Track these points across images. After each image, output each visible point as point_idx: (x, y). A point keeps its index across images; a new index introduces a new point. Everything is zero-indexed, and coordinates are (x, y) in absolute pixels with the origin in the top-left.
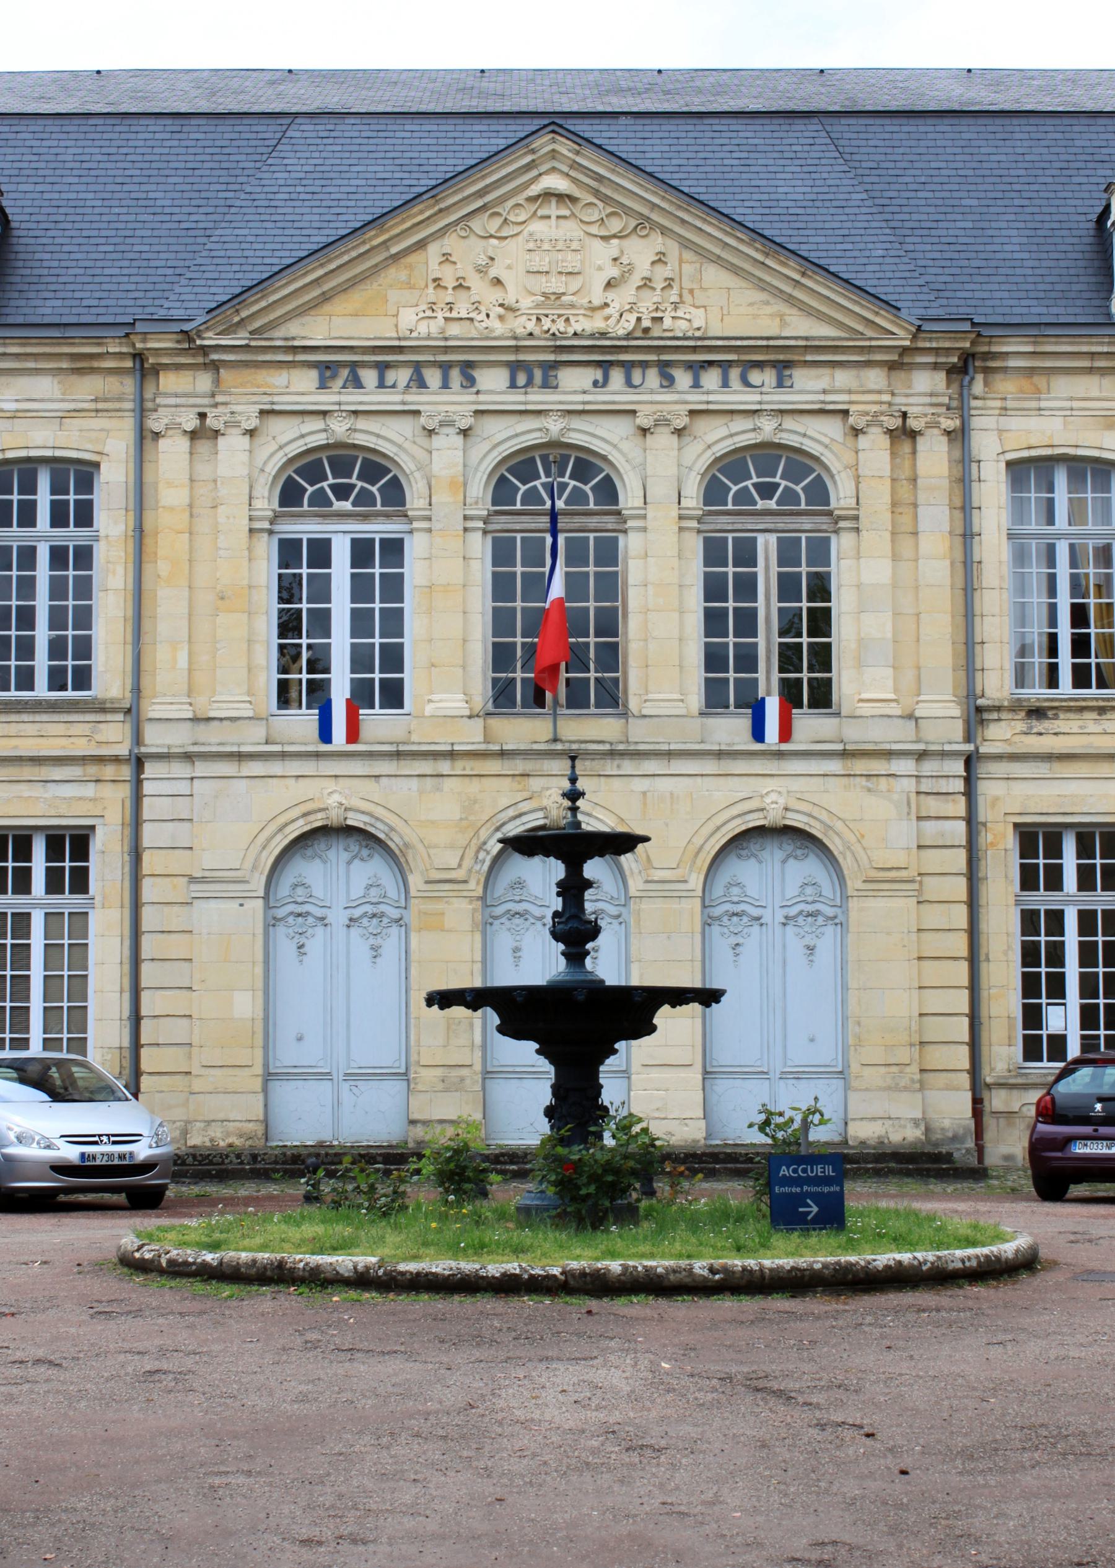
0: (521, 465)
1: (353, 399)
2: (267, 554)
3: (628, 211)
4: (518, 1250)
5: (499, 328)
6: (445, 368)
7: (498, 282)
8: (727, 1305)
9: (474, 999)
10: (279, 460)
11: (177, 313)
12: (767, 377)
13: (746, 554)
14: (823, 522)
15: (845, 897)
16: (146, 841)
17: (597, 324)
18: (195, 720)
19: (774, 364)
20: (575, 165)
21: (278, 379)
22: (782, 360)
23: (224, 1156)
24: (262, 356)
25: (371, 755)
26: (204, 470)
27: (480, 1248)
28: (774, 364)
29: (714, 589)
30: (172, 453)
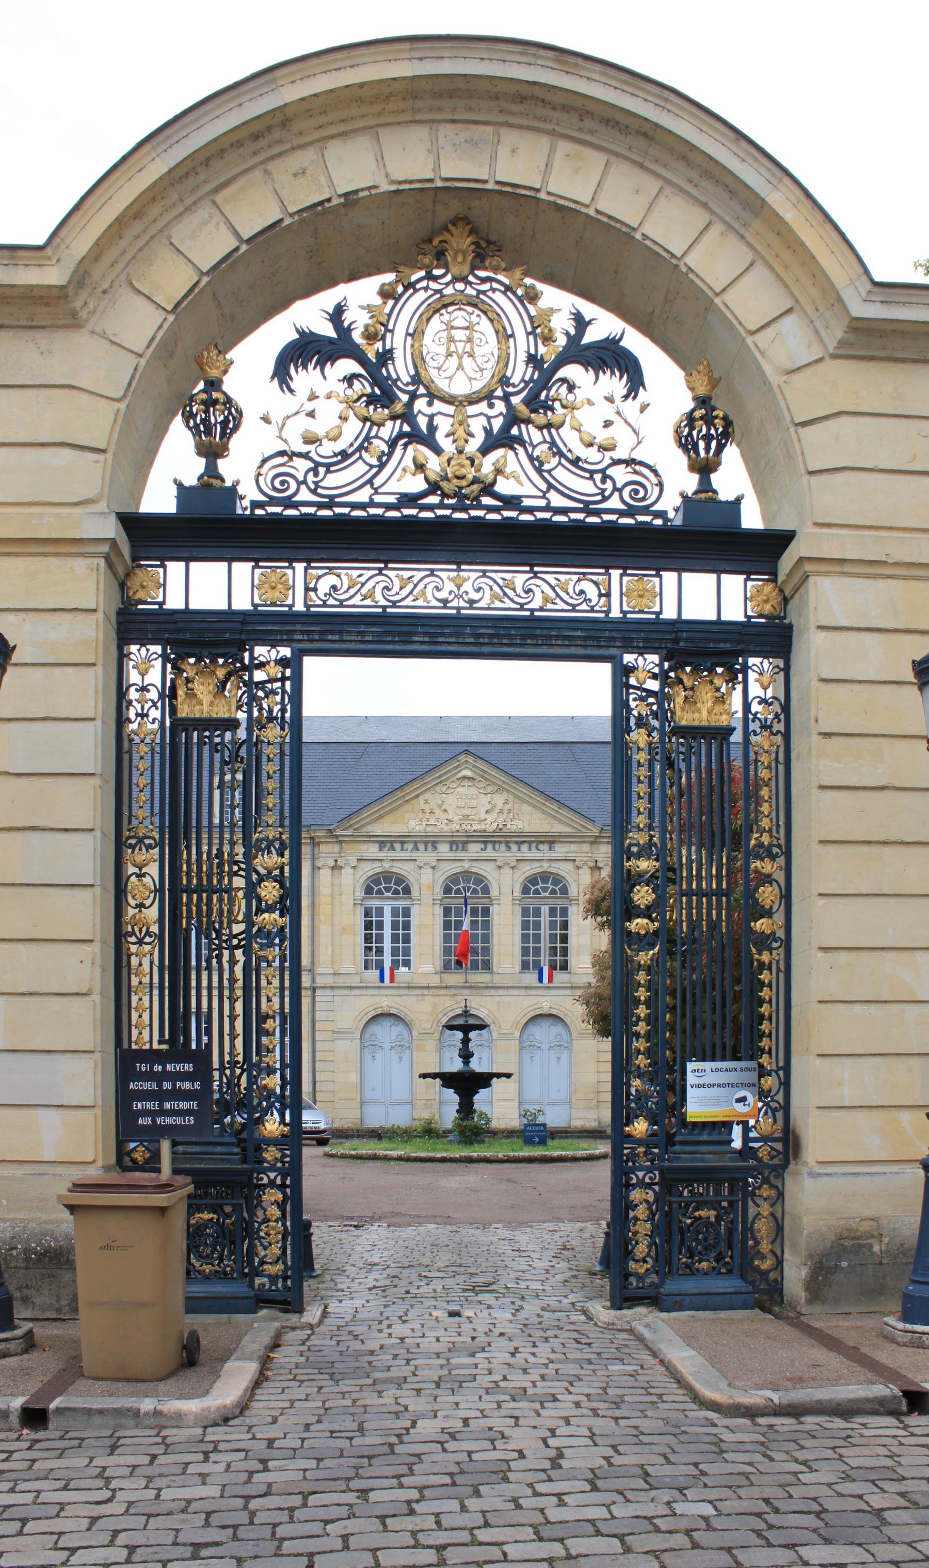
0: (454, 879)
1: (392, 855)
2: (360, 912)
3: (494, 784)
4: (446, 1151)
5: (446, 828)
6: (426, 843)
7: (445, 810)
8: (508, 1165)
9: (434, 1076)
10: (364, 877)
11: (326, 822)
12: (545, 847)
13: (537, 913)
14: (565, 901)
15: (571, 1040)
16: (317, 1018)
17: (482, 827)
18: (334, 974)
19: (548, 842)
20: (475, 766)
21: (364, 847)
22: (551, 841)
23: (347, 1130)
24: (356, 839)
25: (399, 987)
26: (337, 881)
27: (435, 1150)
28: (548, 842)
29: (525, 925)
30: (325, 875)
